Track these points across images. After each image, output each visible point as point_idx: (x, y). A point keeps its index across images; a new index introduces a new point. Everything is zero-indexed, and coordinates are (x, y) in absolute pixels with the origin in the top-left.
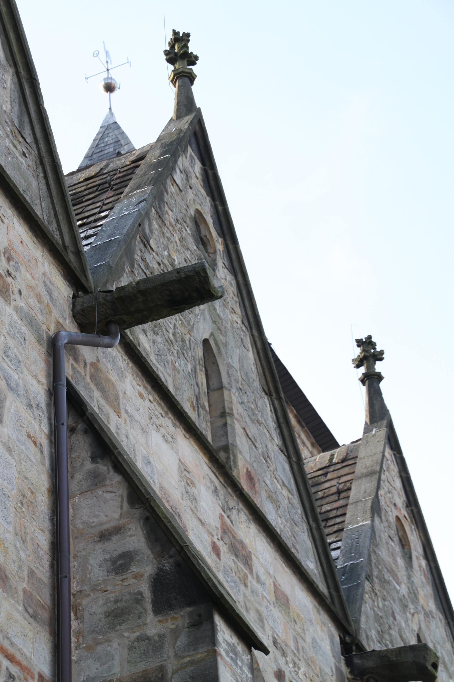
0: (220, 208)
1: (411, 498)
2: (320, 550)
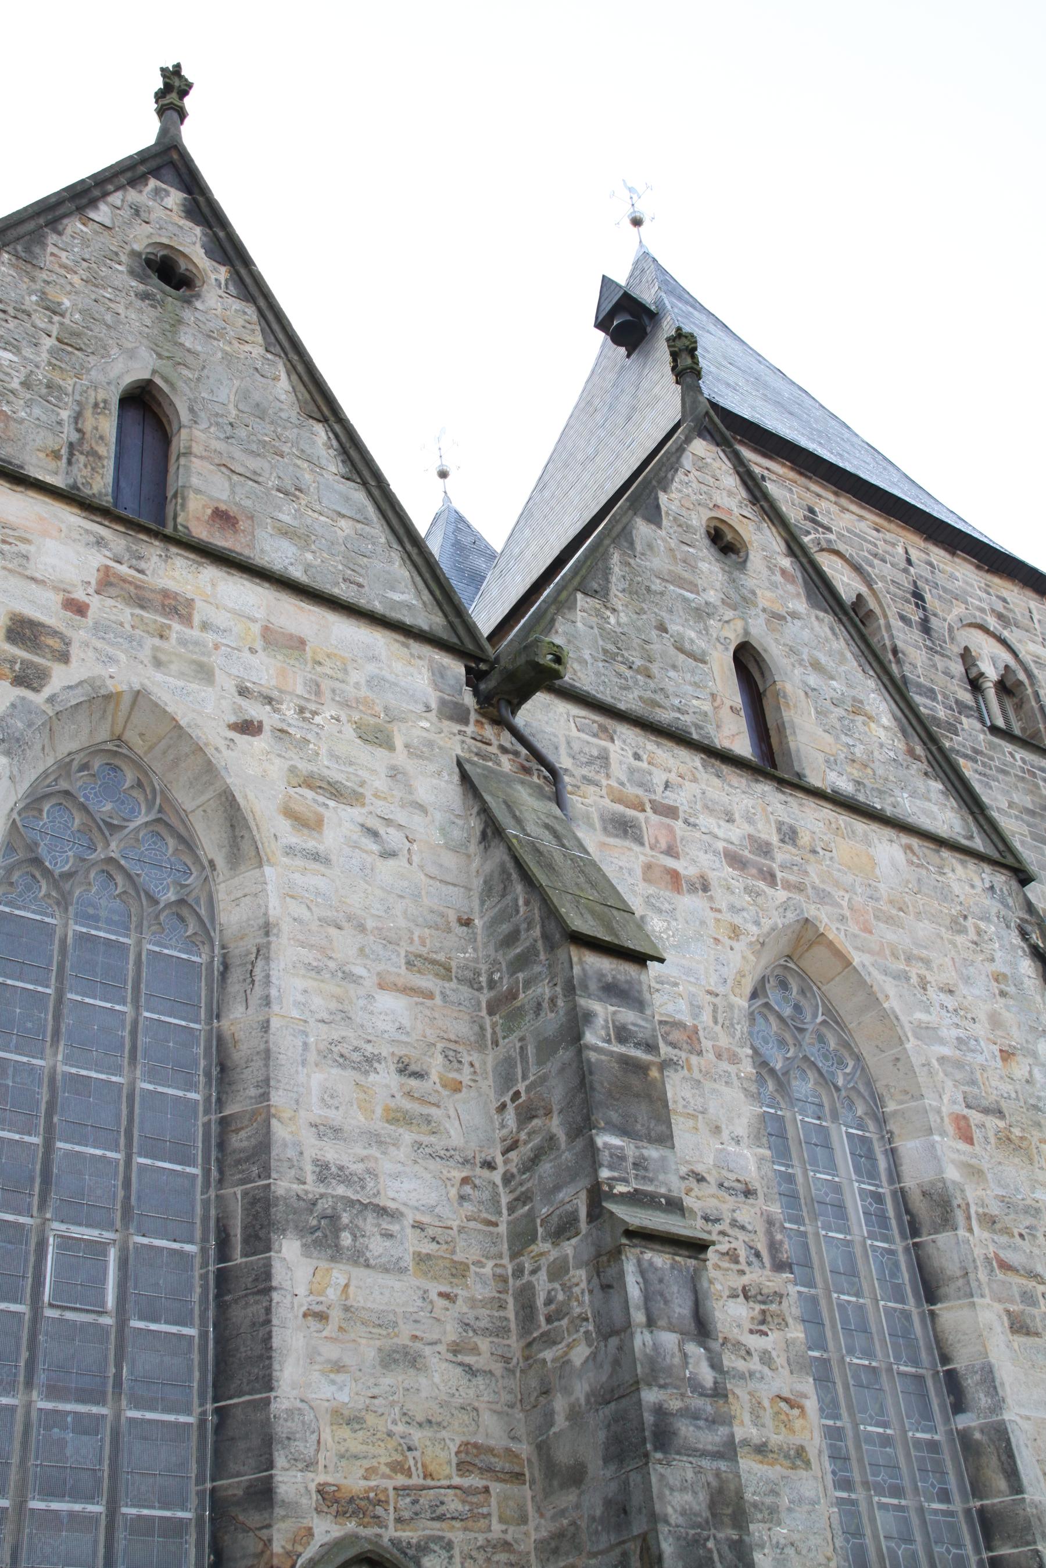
0: (221, 234)
1: (758, 494)
2: (427, 576)
